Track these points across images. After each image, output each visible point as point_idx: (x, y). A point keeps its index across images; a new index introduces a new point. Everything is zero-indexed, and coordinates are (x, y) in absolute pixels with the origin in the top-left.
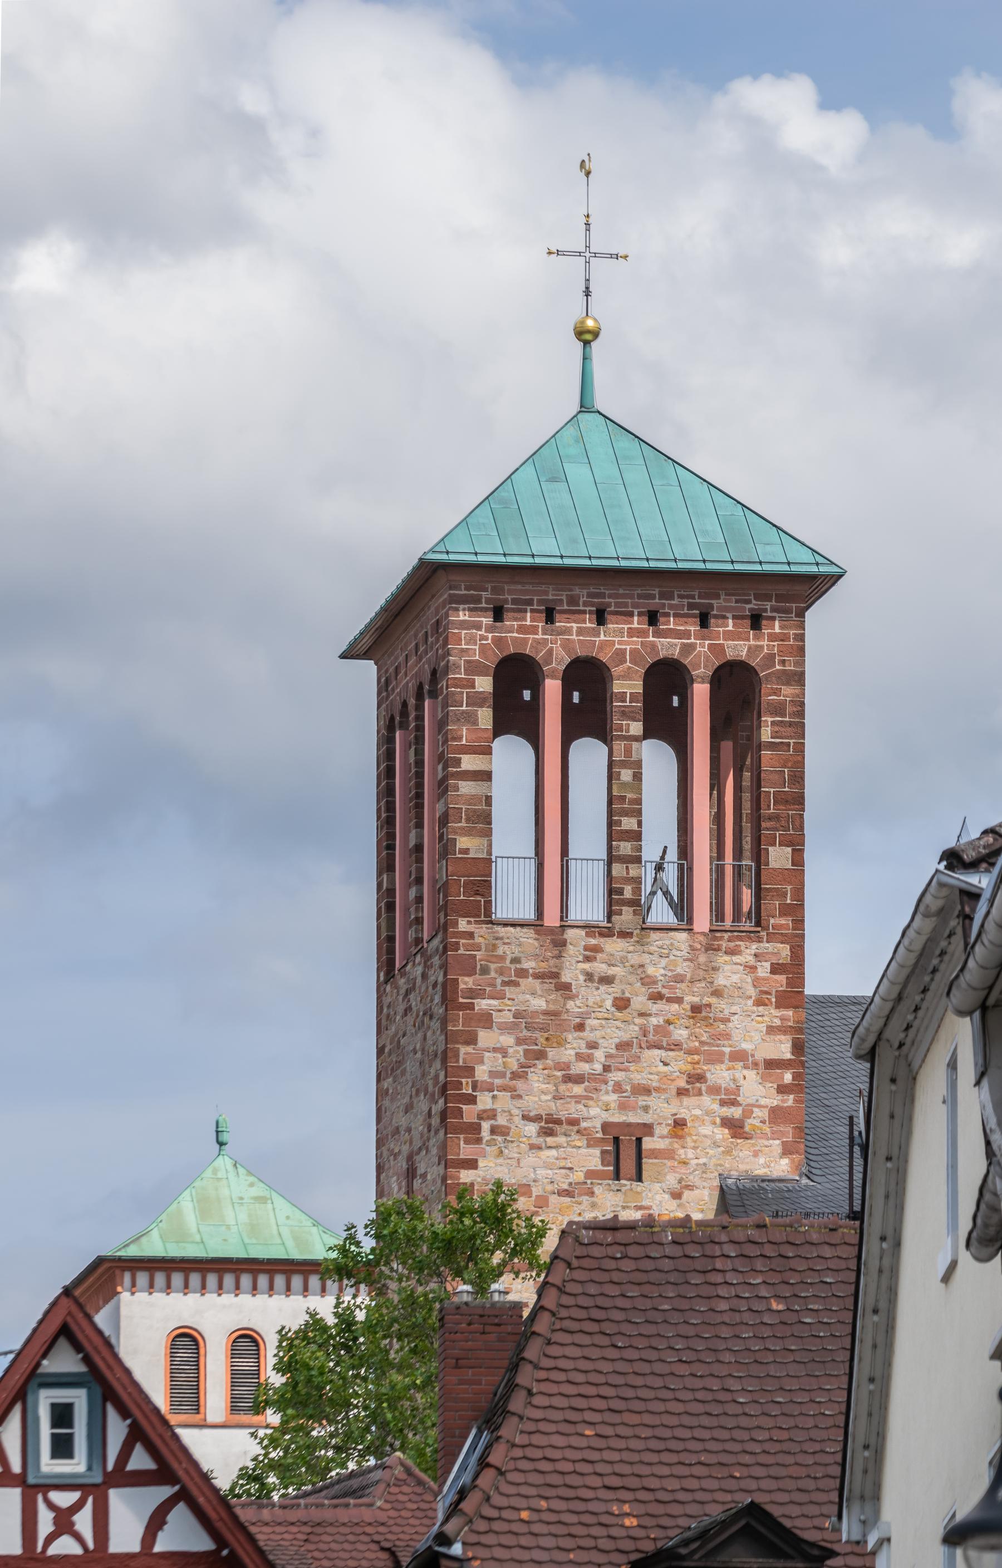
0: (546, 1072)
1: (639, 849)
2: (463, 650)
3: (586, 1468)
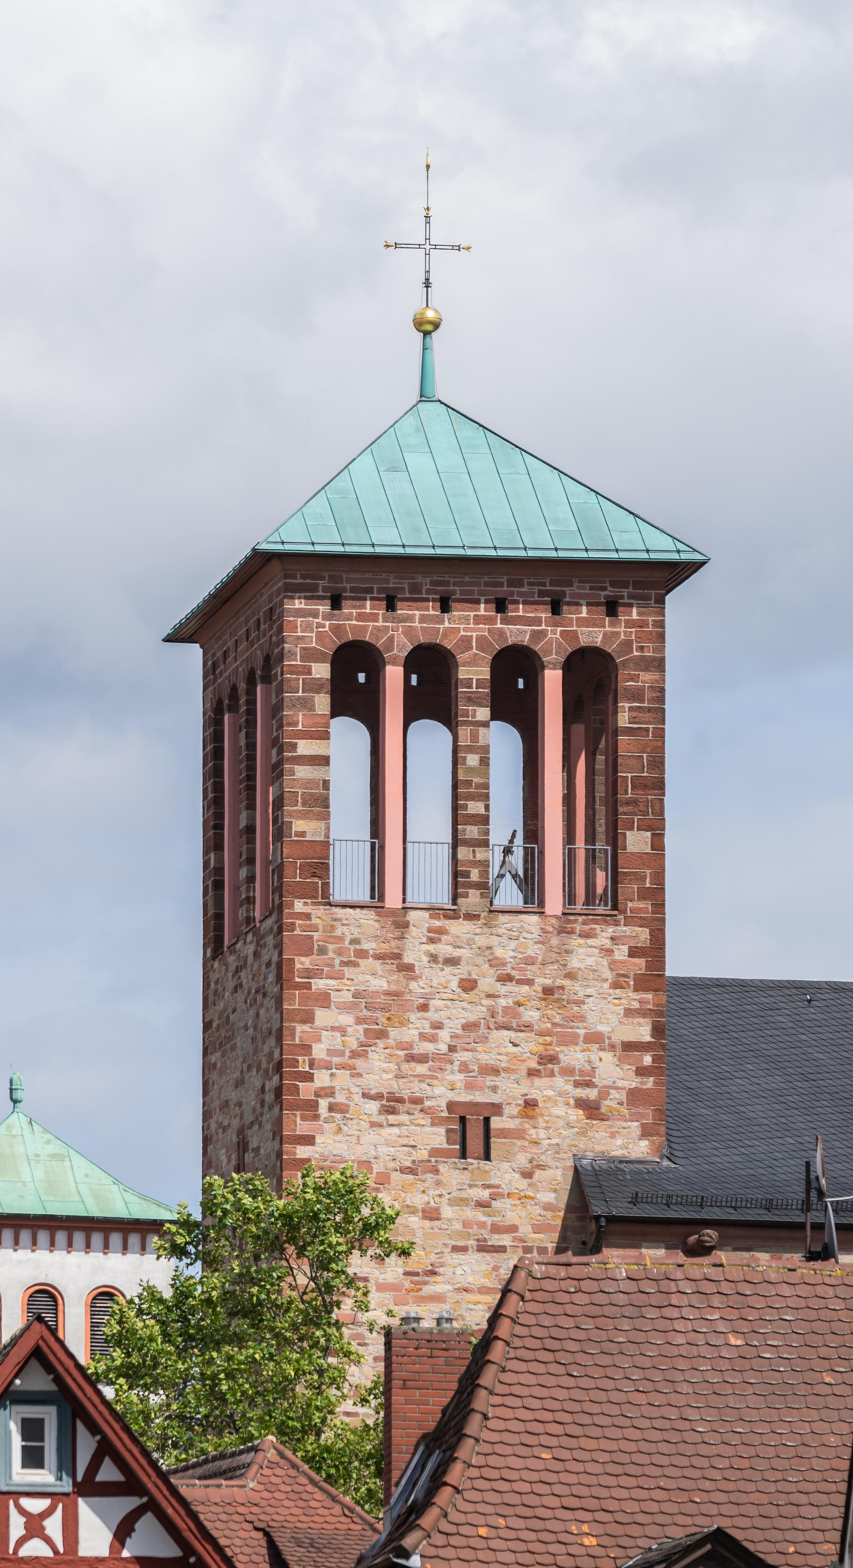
0: (387, 1051)
1: (487, 833)
2: (298, 638)
3: (544, 1489)
